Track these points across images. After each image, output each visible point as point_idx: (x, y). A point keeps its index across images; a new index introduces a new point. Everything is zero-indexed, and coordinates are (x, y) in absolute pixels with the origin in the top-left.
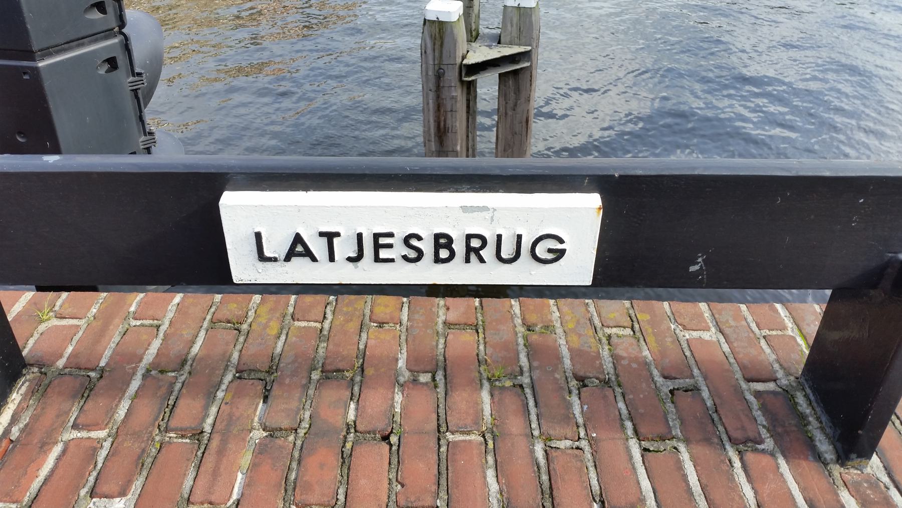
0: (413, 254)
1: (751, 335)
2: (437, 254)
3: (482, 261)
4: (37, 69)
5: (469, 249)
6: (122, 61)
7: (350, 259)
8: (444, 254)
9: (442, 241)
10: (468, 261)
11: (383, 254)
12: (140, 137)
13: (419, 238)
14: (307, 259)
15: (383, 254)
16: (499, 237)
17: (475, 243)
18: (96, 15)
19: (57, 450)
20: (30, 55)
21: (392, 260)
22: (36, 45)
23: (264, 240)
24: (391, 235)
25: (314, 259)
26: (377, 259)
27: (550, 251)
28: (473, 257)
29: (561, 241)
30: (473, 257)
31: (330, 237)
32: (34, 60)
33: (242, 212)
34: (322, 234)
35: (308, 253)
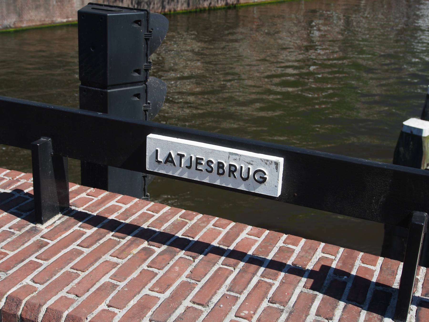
0: (210, 169)
1: (396, 271)
2: (218, 171)
3: (235, 177)
4: (106, 93)
5: (230, 171)
6: (143, 95)
7: (187, 167)
8: (221, 171)
9: (221, 165)
10: (229, 176)
11: (199, 167)
12: (144, 104)
13: (212, 163)
14: (172, 164)
15: (199, 167)
16: (241, 167)
17: (233, 169)
18: (136, 74)
19: (10, 272)
20: (106, 87)
21: (202, 170)
22: (109, 83)
23: (159, 153)
24: (202, 159)
25: (174, 165)
26: (197, 169)
27: (261, 177)
28: (232, 175)
29: (265, 174)
30: (232, 175)
31: (182, 156)
32: (106, 89)
33: (157, 143)
34: (178, 154)
35: (172, 162)
